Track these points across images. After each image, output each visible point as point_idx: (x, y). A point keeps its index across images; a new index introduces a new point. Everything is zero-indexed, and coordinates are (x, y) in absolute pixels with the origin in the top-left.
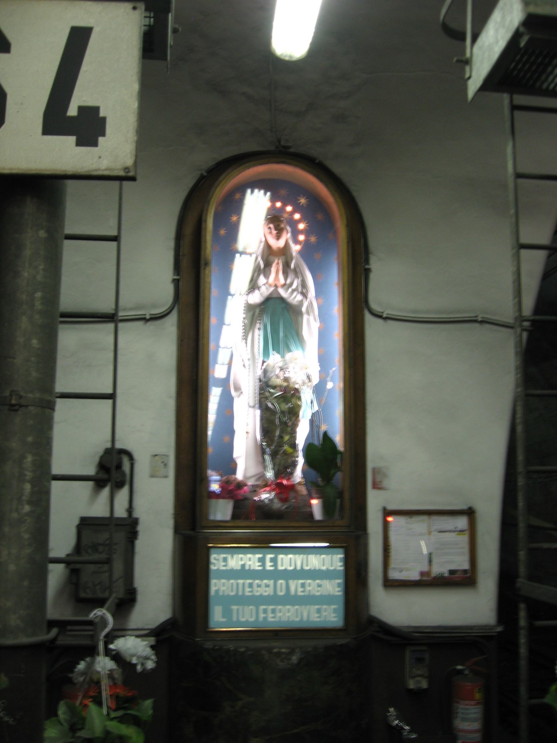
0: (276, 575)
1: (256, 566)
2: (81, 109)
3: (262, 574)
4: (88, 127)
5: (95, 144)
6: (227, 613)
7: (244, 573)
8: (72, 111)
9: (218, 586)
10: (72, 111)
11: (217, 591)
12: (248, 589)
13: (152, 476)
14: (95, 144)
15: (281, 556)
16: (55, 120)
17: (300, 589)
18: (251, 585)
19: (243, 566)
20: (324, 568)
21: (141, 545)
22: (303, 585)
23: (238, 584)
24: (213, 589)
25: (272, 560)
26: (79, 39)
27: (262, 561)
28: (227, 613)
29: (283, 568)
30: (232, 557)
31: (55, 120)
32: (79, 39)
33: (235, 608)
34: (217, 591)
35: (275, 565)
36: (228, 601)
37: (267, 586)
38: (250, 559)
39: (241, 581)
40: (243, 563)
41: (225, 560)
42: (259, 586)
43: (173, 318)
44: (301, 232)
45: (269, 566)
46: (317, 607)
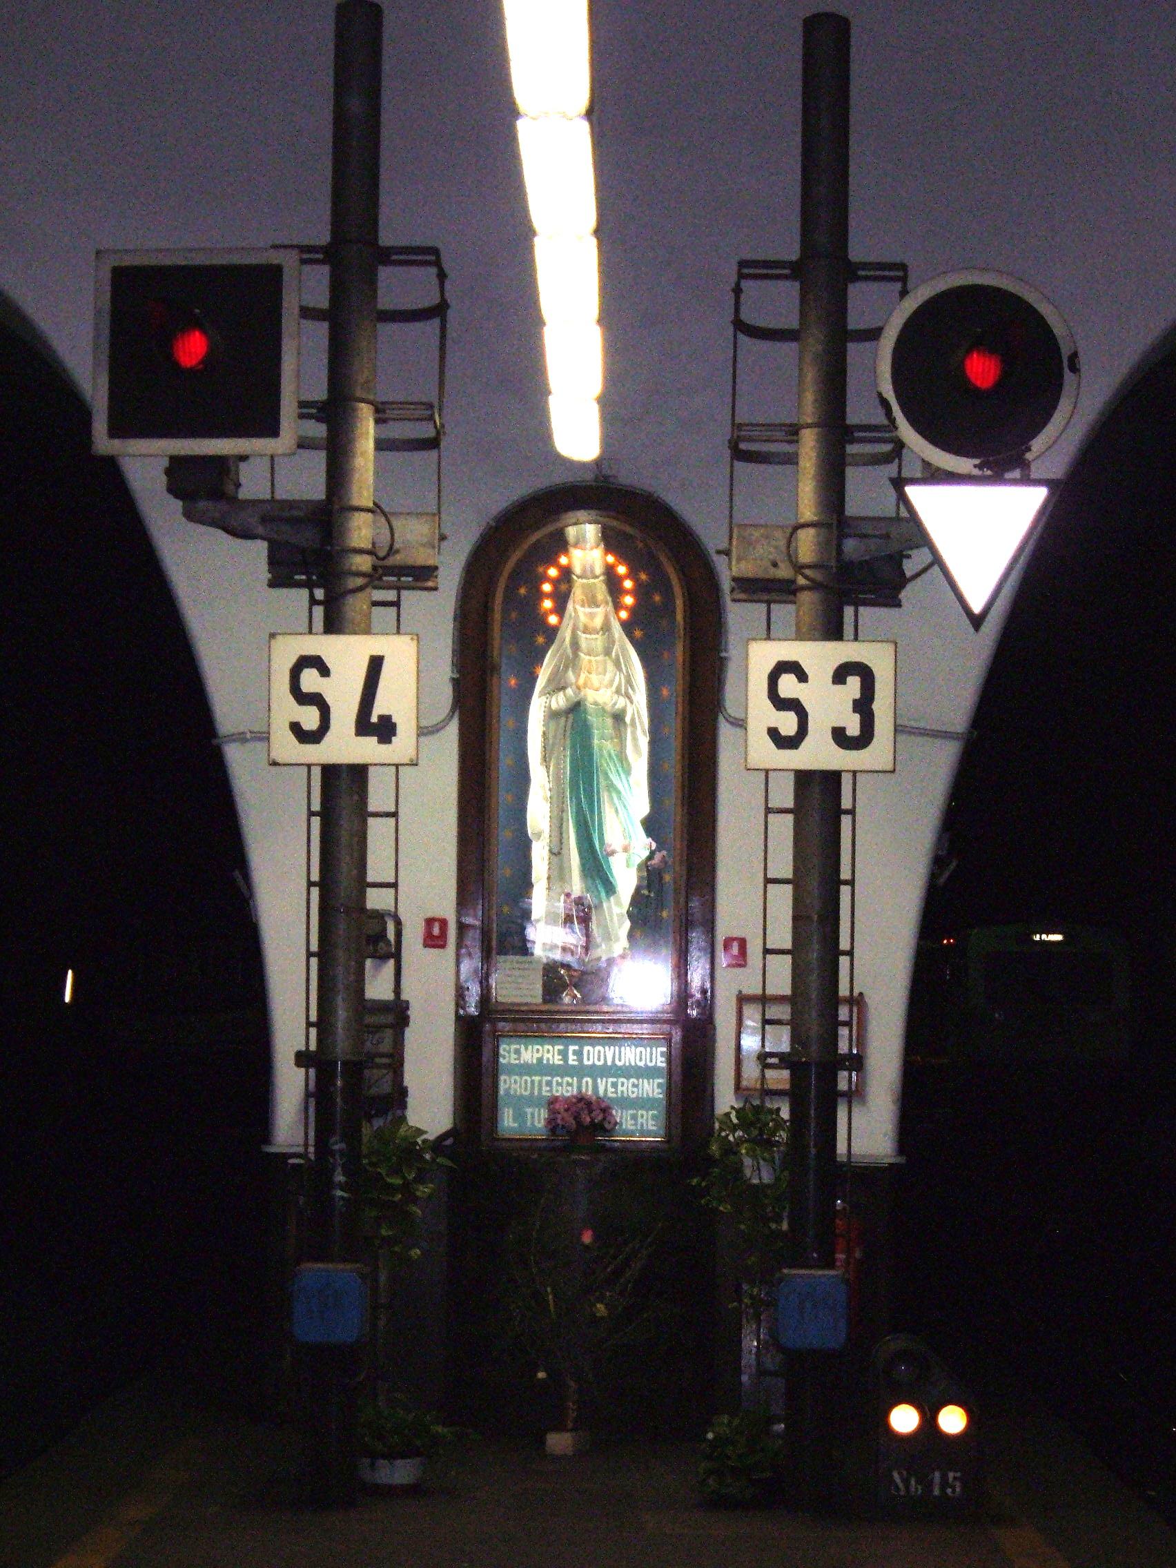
0: (580, 1071)
1: (557, 1060)
2: (381, 717)
3: (565, 1070)
4: (385, 730)
5: (390, 742)
6: (519, 1116)
7: (542, 1068)
8: (374, 719)
9: (509, 1084)
10: (374, 719)
11: (507, 1091)
12: (545, 1088)
13: (98, 253)
14: (390, 742)
15: (586, 1048)
16: (364, 726)
17: (611, 1090)
18: (549, 1084)
19: (540, 1060)
20: (642, 1064)
21: (412, 1035)
22: (614, 1085)
23: (533, 1082)
24: (502, 1087)
25: (575, 1052)
26: (376, 664)
27: (564, 1054)
28: (519, 1116)
29: (590, 1063)
30: (526, 1049)
31: (364, 726)
32: (376, 664)
33: (529, 1110)
34: (507, 1091)
35: (580, 1060)
36: (520, 1103)
37: (569, 1084)
38: (548, 1051)
39: (537, 1078)
40: (539, 1055)
41: (518, 1052)
42: (558, 1084)
43: (453, 729)
44: (626, 608)
45: (572, 1059)
46: (631, 1112)
